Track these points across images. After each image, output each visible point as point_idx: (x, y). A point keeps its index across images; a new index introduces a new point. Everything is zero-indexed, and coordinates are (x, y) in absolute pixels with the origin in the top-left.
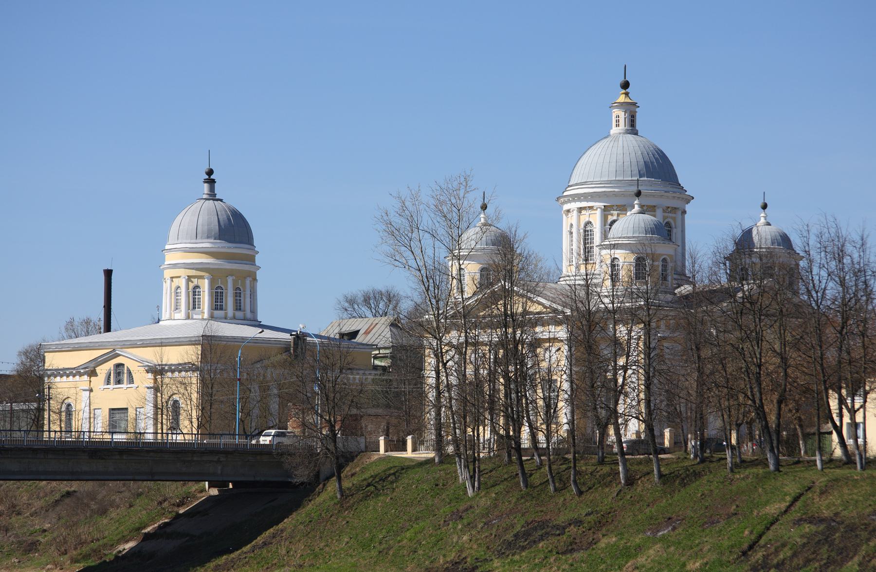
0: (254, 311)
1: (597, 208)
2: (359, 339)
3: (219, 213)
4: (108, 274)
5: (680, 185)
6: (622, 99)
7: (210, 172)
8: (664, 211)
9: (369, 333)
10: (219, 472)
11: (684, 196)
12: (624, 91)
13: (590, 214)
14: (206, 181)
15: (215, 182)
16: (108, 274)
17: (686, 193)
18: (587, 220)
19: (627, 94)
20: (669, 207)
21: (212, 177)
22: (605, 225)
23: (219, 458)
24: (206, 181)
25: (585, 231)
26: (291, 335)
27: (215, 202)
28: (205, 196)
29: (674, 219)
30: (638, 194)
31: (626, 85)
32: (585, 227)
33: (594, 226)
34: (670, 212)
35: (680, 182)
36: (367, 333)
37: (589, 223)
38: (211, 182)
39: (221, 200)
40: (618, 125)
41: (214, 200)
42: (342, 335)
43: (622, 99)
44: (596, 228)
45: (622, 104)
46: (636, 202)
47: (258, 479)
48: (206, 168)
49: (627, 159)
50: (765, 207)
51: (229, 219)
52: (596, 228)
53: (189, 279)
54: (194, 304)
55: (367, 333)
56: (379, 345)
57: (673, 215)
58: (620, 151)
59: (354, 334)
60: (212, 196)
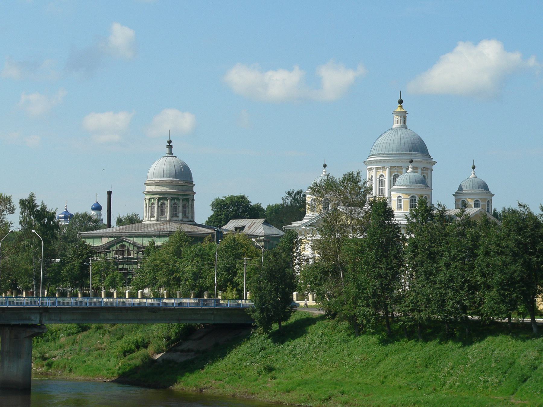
0: (193, 217)
1: (387, 168)
2: (246, 231)
3: (175, 164)
4: (110, 193)
5: (429, 155)
6: (399, 109)
7: (170, 142)
8: (422, 170)
9: (251, 227)
10: (213, 319)
11: (432, 162)
12: (399, 105)
13: (382, 171)
14: (168, 147)
15: (172, 147)
16: (110, 193)
17: (433, 160)
18: (381, 174)
19: (401, 107)
20: (424, 168)
21: (171, 144)
22: (391, 177)
23: (213, 312)
24: (168, 147)
25: (380, 180)
26: (215, 230)
27: (173, 158)
28: (167, 155)
29: (427, 174)
30: (411, 162)
31: (401, 102)
32: (380, 177)
33: (385, 177)
34: (425, 170)
35: (430, 154)
36: (250, 227)
37: (382, 176)
38: (170, 147)
39: (176, 157)
40: (397, 123)
41: (172, 157)
42: (236, 229)
43: (399, 109)
44: (386, 178)
45: (399, 112)
46: (410, 166)
47: (232, 322)
48: (168, 139)
49: (403, 142)
50: (474, 168)
51: (180, 167)
52: (386, 178)
53: (159, 199)
54: (161, 212)
55: (250, 227)
56: (259, 235)
57: (427, 172)
58: (399, 137)
59: (243, 228)
60: (171, 154)
